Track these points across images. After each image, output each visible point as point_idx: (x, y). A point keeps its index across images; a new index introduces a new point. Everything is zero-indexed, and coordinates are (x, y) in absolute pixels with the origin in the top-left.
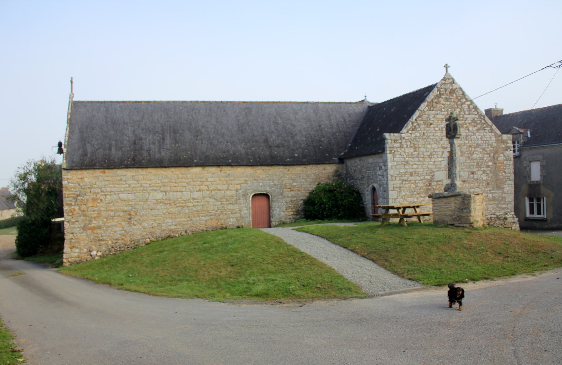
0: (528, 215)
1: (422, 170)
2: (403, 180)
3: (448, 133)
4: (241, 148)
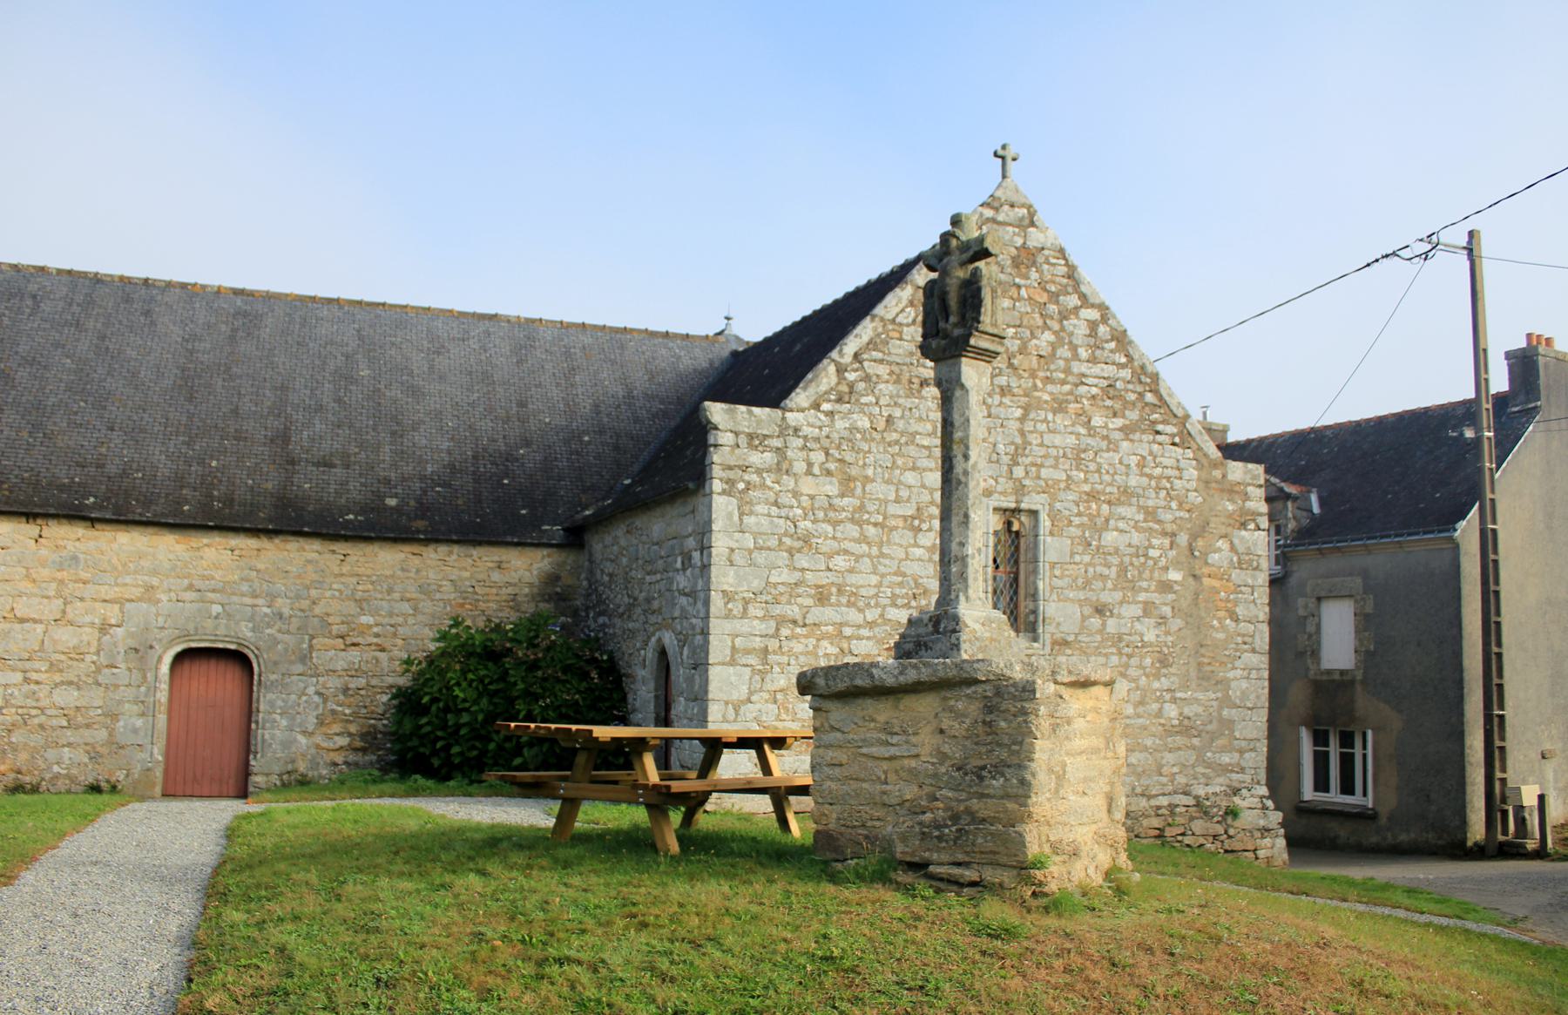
0: (1308, 793)
1: (874, 579)
2: (781, 621)
3: (932, 329)
4: (161, 458)
